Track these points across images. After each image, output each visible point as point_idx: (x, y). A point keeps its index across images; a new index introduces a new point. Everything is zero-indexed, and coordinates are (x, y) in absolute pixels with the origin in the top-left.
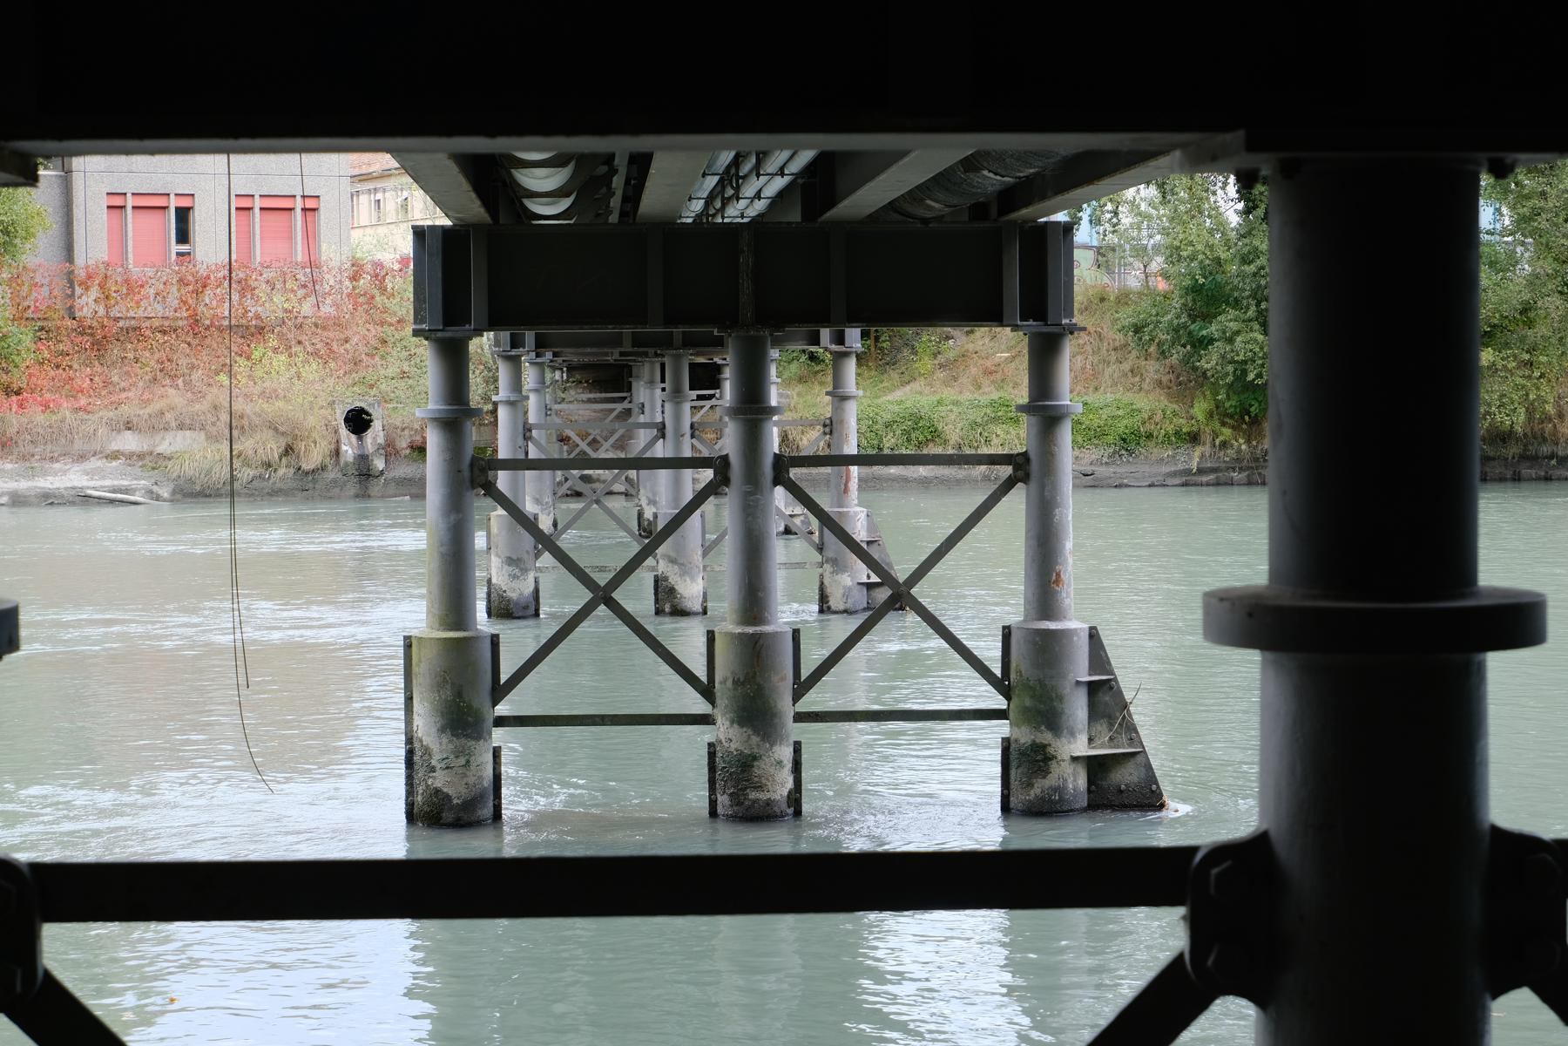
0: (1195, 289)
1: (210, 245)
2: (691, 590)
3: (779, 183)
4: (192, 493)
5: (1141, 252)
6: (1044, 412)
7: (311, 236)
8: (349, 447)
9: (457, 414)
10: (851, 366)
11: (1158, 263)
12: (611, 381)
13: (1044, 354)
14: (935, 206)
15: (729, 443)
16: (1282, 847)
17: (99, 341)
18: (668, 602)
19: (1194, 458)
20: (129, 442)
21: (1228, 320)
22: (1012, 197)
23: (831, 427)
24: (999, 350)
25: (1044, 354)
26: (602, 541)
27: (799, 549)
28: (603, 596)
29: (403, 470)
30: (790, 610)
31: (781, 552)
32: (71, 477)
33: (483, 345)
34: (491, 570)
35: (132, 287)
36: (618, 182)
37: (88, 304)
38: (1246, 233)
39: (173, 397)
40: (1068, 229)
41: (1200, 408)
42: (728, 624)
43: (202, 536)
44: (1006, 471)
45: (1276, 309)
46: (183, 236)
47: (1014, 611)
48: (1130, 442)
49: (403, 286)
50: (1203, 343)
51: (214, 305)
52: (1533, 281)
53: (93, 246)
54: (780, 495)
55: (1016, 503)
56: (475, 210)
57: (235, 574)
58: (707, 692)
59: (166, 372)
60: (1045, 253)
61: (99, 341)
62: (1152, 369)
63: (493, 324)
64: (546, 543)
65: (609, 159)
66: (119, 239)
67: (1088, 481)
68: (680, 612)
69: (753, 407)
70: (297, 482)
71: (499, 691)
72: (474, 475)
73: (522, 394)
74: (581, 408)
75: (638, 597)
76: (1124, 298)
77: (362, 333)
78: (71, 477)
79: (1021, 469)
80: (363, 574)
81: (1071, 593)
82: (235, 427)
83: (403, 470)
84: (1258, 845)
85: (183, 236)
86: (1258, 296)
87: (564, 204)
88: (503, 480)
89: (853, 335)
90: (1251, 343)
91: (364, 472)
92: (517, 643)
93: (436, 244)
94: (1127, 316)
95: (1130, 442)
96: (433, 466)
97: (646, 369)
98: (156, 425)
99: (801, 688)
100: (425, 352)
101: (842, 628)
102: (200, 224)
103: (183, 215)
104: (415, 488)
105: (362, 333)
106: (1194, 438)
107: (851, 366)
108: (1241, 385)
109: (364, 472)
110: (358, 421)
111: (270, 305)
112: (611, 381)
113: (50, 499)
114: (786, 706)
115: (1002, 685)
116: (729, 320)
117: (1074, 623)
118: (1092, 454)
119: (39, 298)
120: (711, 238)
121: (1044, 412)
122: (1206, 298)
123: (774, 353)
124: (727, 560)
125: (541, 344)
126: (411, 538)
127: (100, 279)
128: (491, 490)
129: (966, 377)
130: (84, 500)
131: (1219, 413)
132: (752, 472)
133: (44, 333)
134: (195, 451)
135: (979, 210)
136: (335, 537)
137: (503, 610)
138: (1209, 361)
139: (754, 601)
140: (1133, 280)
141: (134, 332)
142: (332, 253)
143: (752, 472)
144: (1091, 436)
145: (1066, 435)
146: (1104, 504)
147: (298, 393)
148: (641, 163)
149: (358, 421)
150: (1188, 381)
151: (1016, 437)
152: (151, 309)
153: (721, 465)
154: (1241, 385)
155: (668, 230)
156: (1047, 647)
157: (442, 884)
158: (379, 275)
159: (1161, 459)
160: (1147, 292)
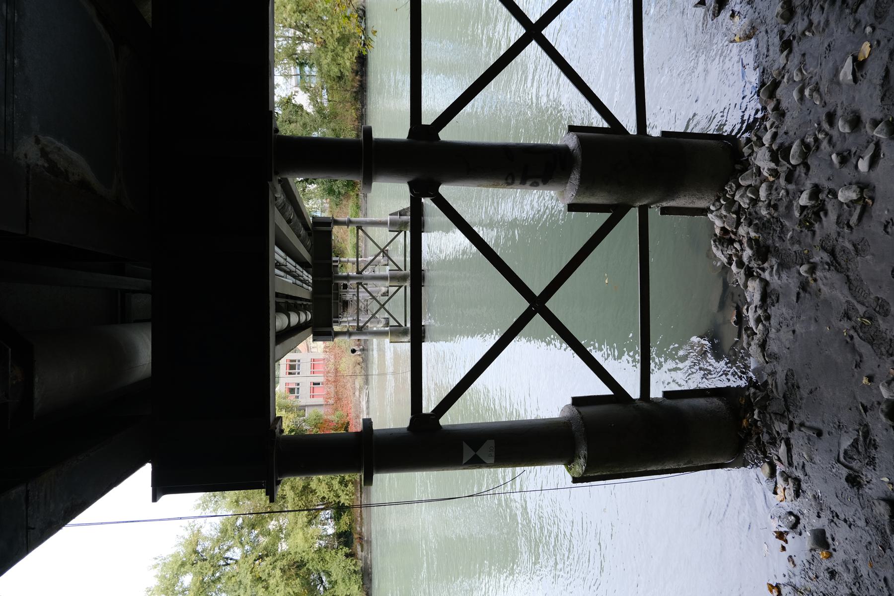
0: (329, 193)
1: (320, 379)
2: (384, 290)
3: (305, 272)
4: (367, 382)
5: (322, 204)
6: (349, 223)
7: (319, 360)
8: (358, 353)
9: (349, 334)
10: (342, 259)
11: (324, 201)
12: (346, 304)
13: (337, 223)
14: (309, 243)
15: (354, 282)
16: (410, 179)
17: (338, 399)
18: (384, 295)
19: (361, 195)
20: (357, 393)
21: (335, 188)
22: (306, 227)
23: (353, 263)
24: (335, 229)
25: (337, 223)
26: (375, 306)
27: (377, 269)
28: (382, 306)
29: (363, 342)
30: (386, 271)
31: (377, 273)
32: (364, 404)
33: (336, 328)
34: (380, 327)
35: (328, 393)
36: (305, 303)
37: (331, 401)
38: (318, 184)
39: (349, 385)
40: (313, 218)
41: (352, 193)
42: (387, 283)
43: (374, 380)
44: (360, 232)
45: (334, 177)
46: (319, 384)
47: (385, 230)
48: (358, 207)
49: (328, 343)
50: (339, 193)
51: (331, 379)
52: (327, 128)
53: (321, 401)
54: (364, 273)
55: (370, 230)
56: (309, 330)
57: (382, 374)
58: (400, 287)
59: (344, 387)
60: (318, 222)
61: (338, 399)
62: (344, 202)
63: (331, 326)
64: (374, 316)
65: (277, 303)
66: (319, 396)
67: (366, 215)
68: (388, 292)
69: (348, 278)
70: (365, 362)
71: (400, 326)
72: (360, 330)
73: (347, 321)
74: (351, 310)
75: (383, 300)
76: (331, 207)
77: (337, 350)
78: (364, 404)
79: (359, 228)
80: (381, 350)
81: (383, 219)
82: (354, 375)
83: (363, 342)
84: (409, 183)
85: (319, 384)
86: (330, 182)
87: (309, 313)
88: (361, 324)
89: (334, 259)
90: (340, 181)
91: (363, 350)
92: (392, 322)
93: (316, 337)
94: (334, 207)
95: (358, 207)
96: (363, 338)
97: (344, 297)
98: (354, 388)
99: (400, 269)
100: (336, 340)
101: (390, 262)
102: (316, 380)
103: (314, 384)
104: (366, 341)
105: (337, 350)
106: (357, 195)
107: (342, 259)
108: (347, 185)
109: (363, 350)
110: (353, 351)
111: (331, 367)
112: (346, 304)
113: (368, 408)
114: (403, 272)
115: (400, 232)
116: (331, 282)
117: (388, 218)
118: (360, 214)
119: (330, 411)
120: (315, 284)
121: (349, 223)
122: (330, 192)
123: (340, 274)
124: (379, 283)
125: (338, 317)
126: (375, 341)
127: (326, 399)
128: (362, 327)
129: (342, 237)
130: (368, 401)
131: (353, 190)
132: (360, 279)
133: (336, 409)
134: (359, 381)
135: (310, 235)
136: (375, 354)
137: (387, 324)
138: (343, 191)
139: (384, 278)
140: (327, 205)
141: (337, 393)
142: (322, 356)
143: (360, 279)
144: (357, 215)
145: (353, 219)
146: (369, 212)
147: (348, 362)
148: (278, 295)
149: (353, 351)
150: (347, 196)
151: (353, 228)
152: (332, 390)
153: (358, 284)
154: (347, 185)
155: (314, 293)
156: (393, 223)
157: (417, 336)
158: (326, 347)
159: (361, 200)
160: (329, 203)
